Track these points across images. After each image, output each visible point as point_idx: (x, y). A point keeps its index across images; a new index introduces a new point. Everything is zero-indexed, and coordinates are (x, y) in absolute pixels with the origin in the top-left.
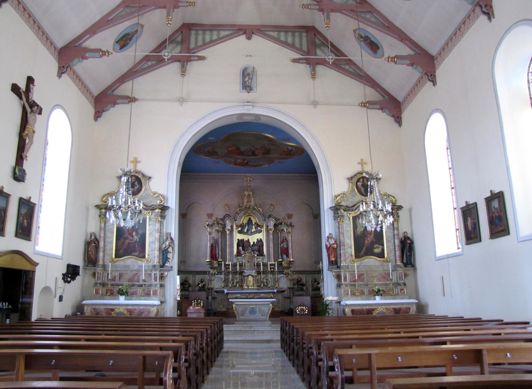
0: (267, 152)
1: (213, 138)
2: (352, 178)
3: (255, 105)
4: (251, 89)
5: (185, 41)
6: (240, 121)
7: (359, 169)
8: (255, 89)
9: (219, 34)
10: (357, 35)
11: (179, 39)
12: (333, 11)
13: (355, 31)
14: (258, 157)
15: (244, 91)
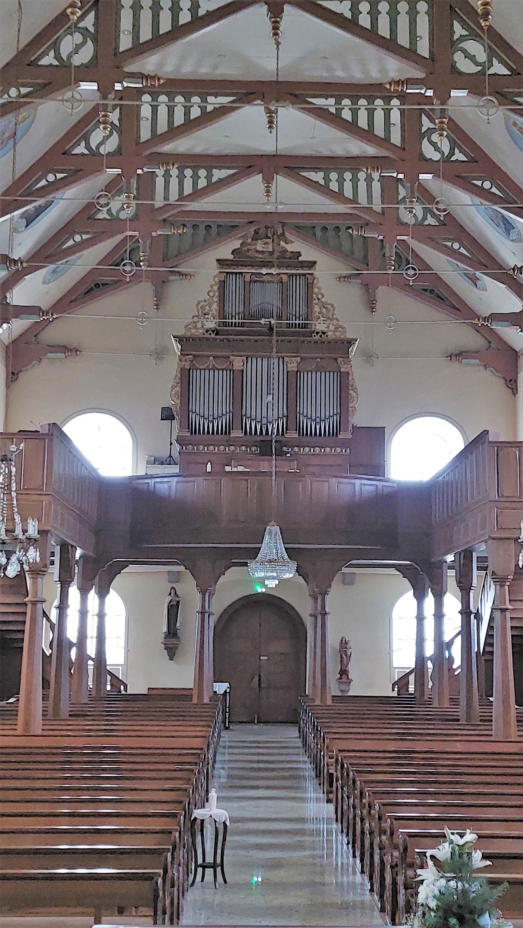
9: (209, 177)
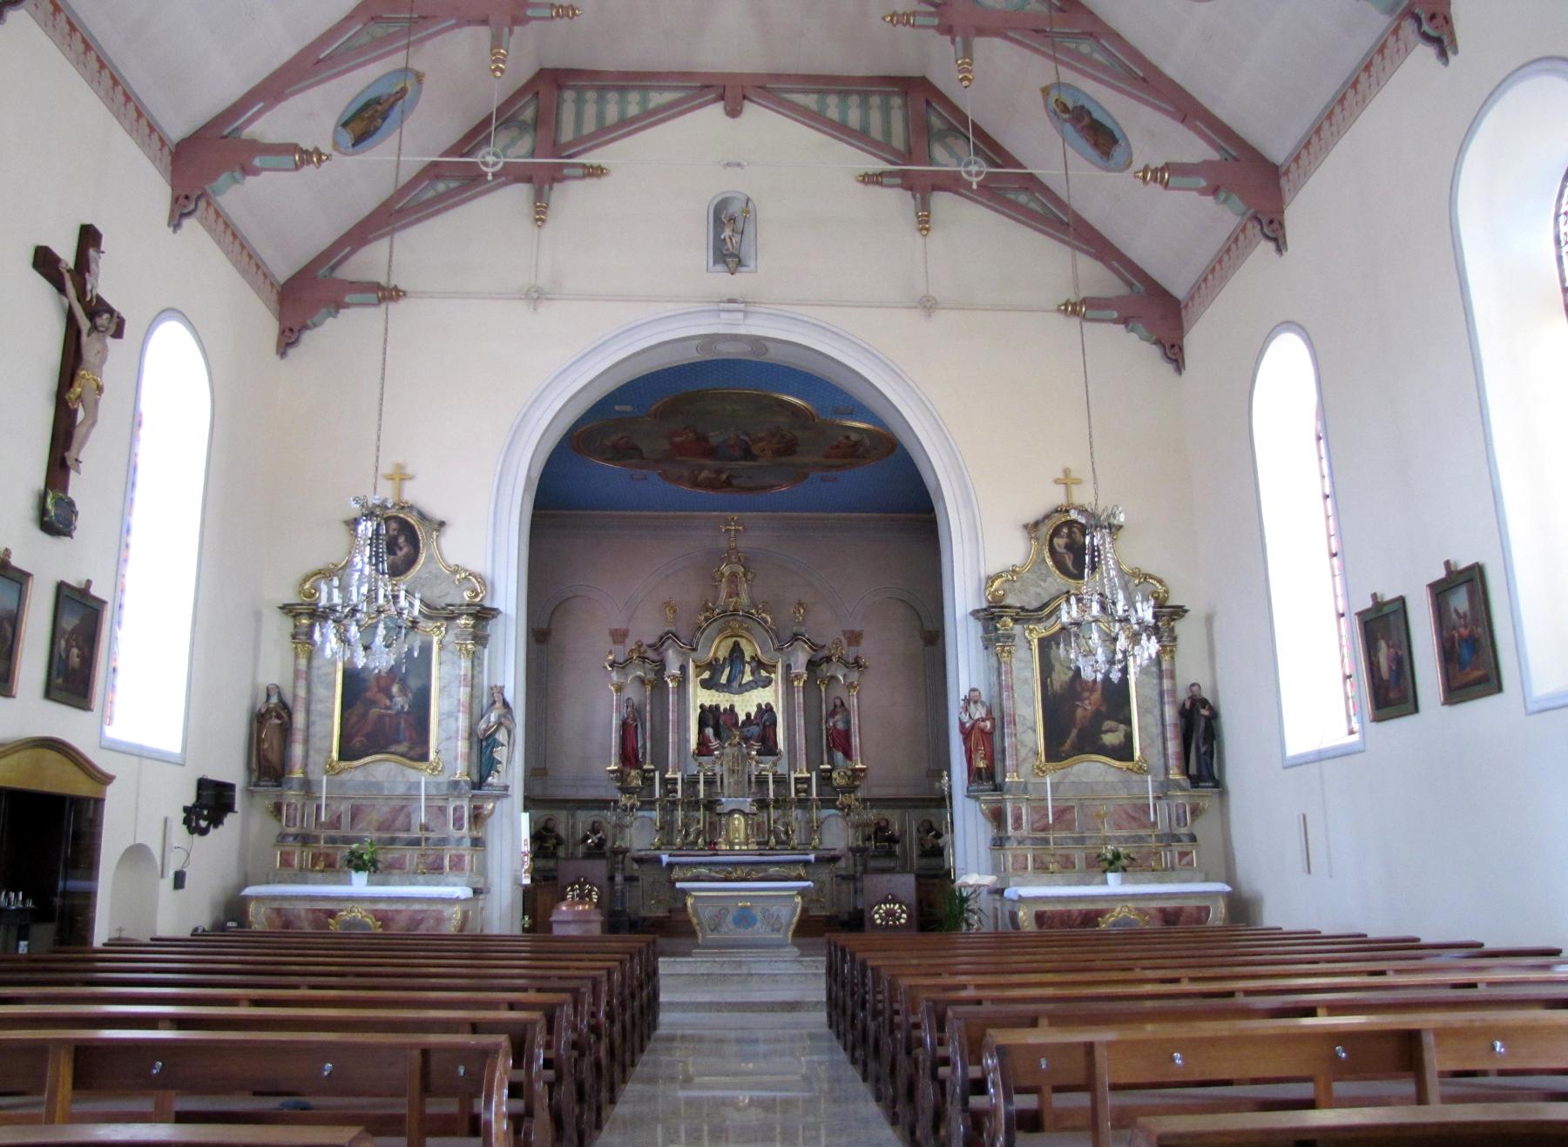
0: (788, 448)
1: (629, 408)
2: (1037, 524)
3: (750, 308)
4: (740, 263)
5: (545, 122)
6: (708, 357)
7: (1057, 497)
8: (752, 264)
9: (644, 101)
10: (1052, 105)
11: (528, 114)
12: (981, 32)
13: (1045, 91)
14: (761, 462)
15: (720, 267)
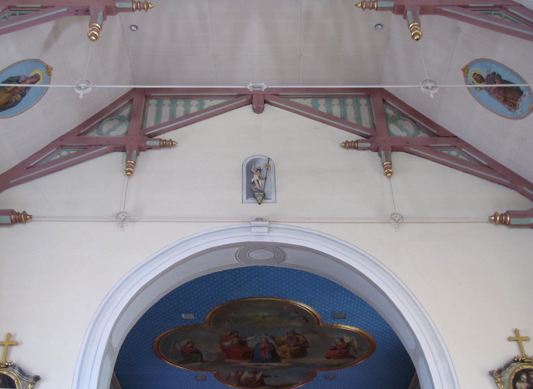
0: (301, 350)
1: (191, 316)
2: (500, 371)
3: (272, 225)
4: (264, 197)
5: (137, 115)
6: (244, 265)
7: (512, 351)
8: (273, 198)
10: (471, 78)
11: (126, 112)
12: (395, 149)
13: (465, 70)
14: (284, 363)
15: (251, 200)
